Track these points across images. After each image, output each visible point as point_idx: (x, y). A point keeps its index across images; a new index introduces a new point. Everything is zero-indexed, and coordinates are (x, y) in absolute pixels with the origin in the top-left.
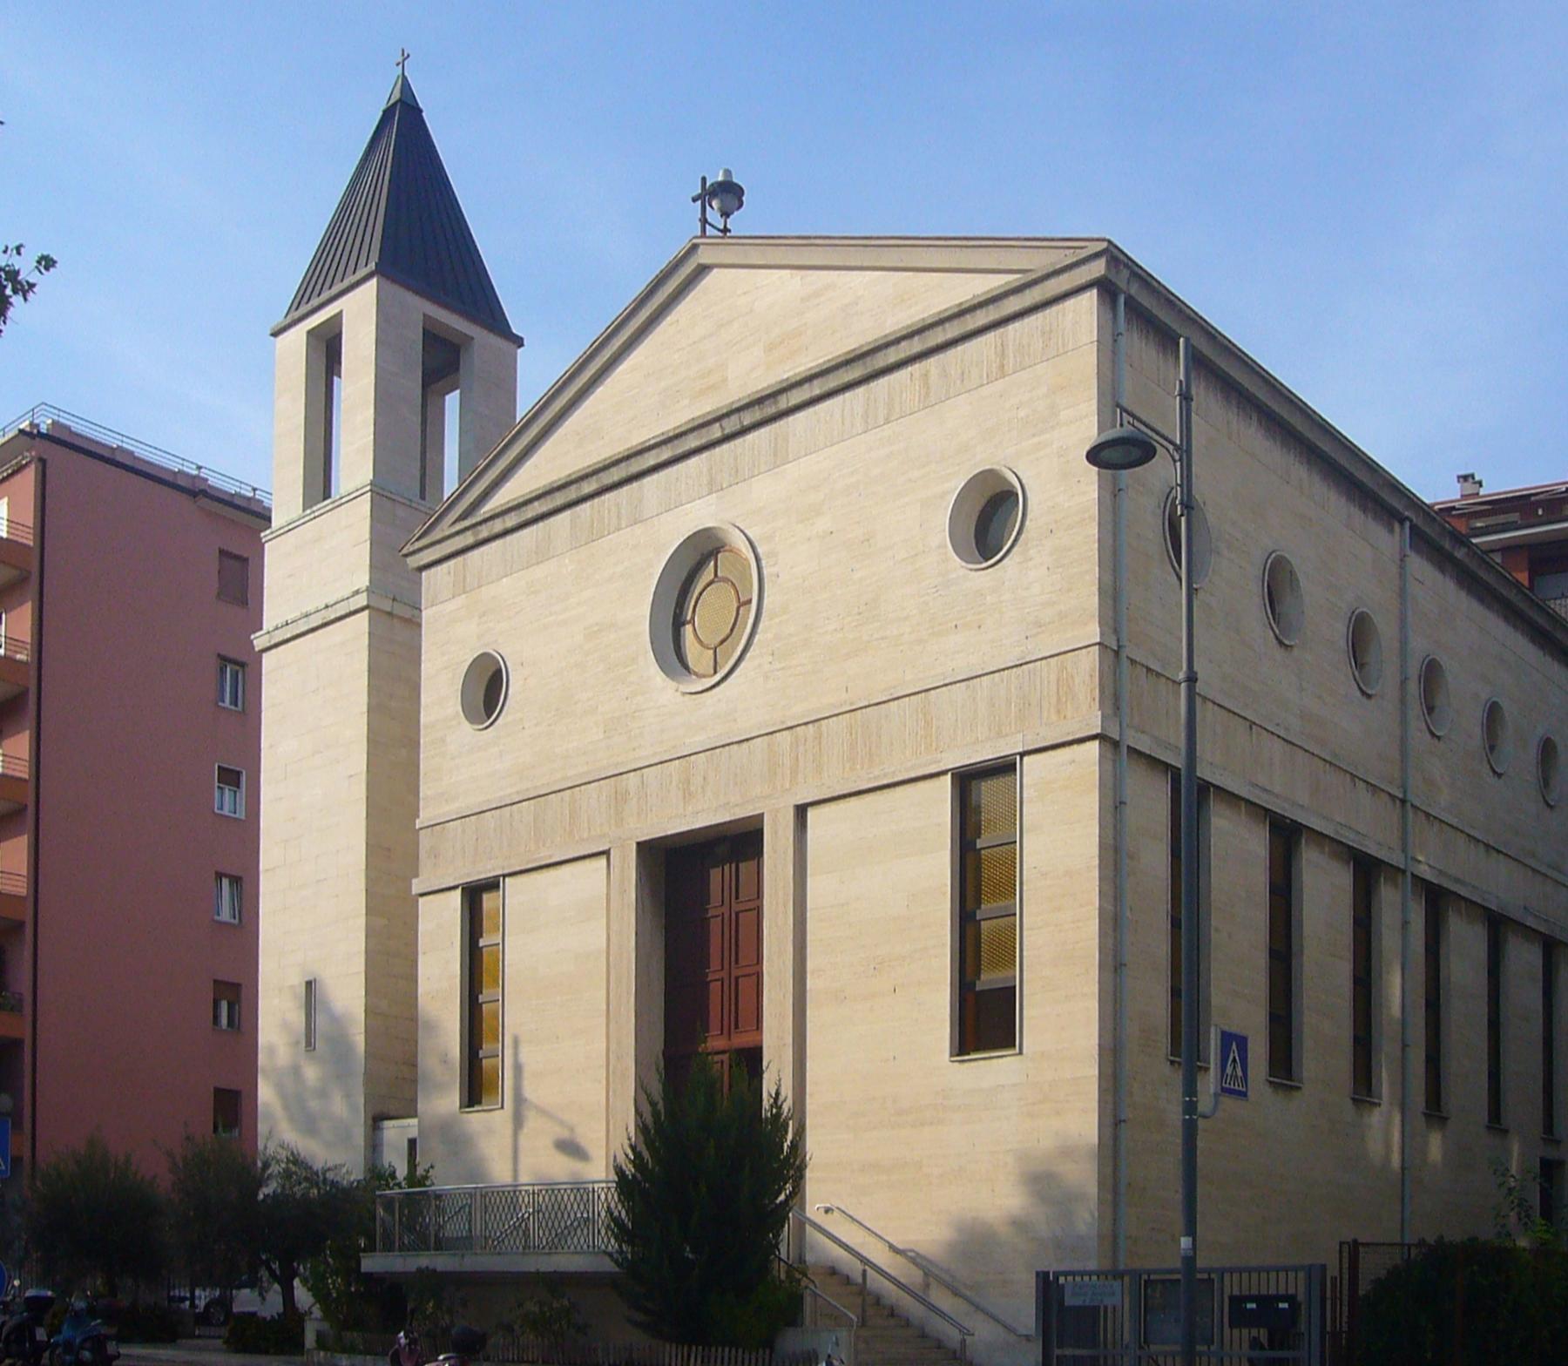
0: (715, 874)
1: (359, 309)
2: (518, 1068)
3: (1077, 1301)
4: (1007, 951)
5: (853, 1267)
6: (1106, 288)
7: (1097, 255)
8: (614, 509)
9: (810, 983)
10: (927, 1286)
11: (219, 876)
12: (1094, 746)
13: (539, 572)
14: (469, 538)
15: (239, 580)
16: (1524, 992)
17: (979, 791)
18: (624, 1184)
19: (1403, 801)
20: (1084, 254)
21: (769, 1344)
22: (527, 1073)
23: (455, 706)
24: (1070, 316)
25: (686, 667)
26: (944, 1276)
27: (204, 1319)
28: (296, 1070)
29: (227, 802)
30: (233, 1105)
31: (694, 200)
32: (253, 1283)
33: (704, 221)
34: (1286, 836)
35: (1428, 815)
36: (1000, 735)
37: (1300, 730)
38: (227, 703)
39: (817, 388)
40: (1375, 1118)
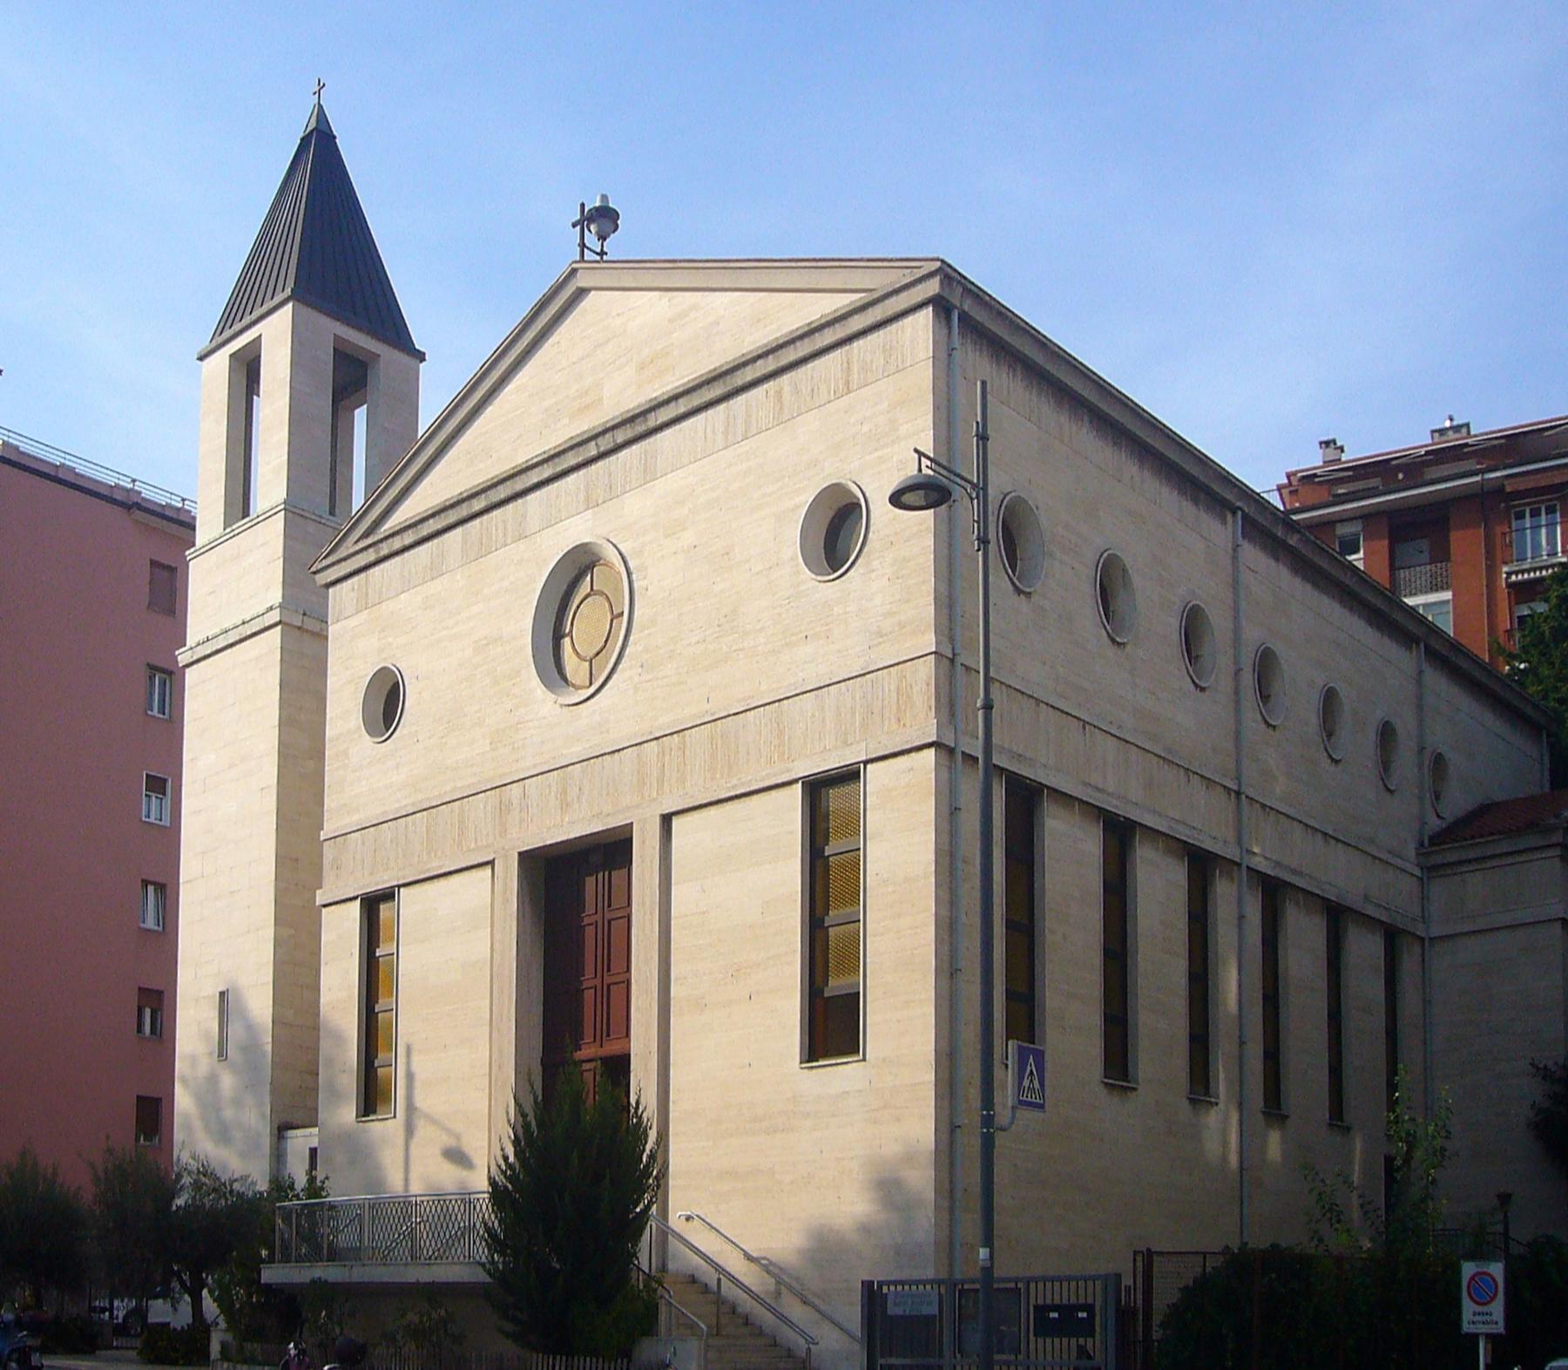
0: (590, 882)
1: (276, 334)
2: (410, 1076)
3: (898, 1311)
4: (852, 957)
5: (710, 1277)
6: (941, 305)
7: (931, 275)
8: (501, 526)
9: (674, 990)
10: (778, 1294)
11: (145, 883)
12: (930, 754)
13: (435, 587)
14: (371, 556)
15: (166, 591)
16: (1364, 985)
17: (827, 799)
18: (498, 1194)
19: (1238, 793)
20: (919, 274)
21: (627, 1354)
22: (418, 1084)
23: (356, 719)
24: (909, 332)
25: (566, 680)
26: (794, 1284)
27: (122, 1330)
28: (213, 1079)
29: (153, 810)
30: (152, 1113)
31: (574, 226)
32: (166, 1294)
33: (583, 246)
34: (1120, 835)
35: (1263, 806)
36: (846, 744)
37: (1130, 725)
38: (155, 712)
39: (682, 407)
40: (1212, 1118)
